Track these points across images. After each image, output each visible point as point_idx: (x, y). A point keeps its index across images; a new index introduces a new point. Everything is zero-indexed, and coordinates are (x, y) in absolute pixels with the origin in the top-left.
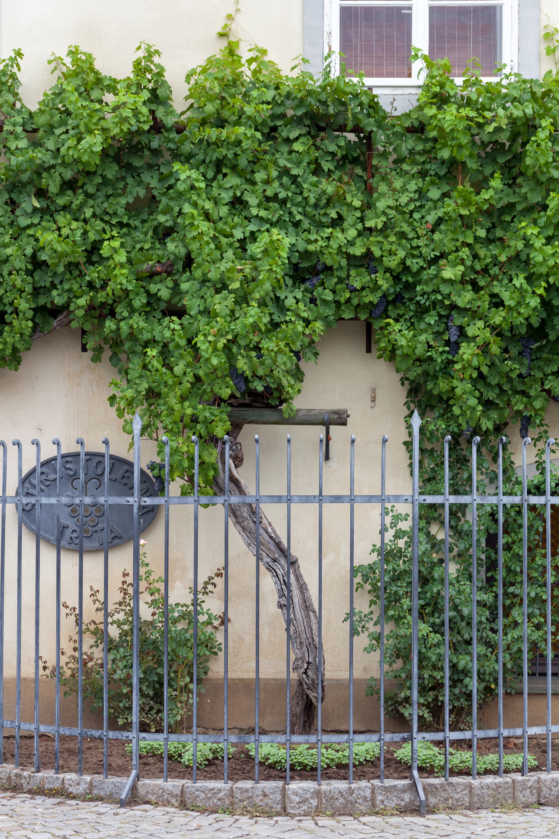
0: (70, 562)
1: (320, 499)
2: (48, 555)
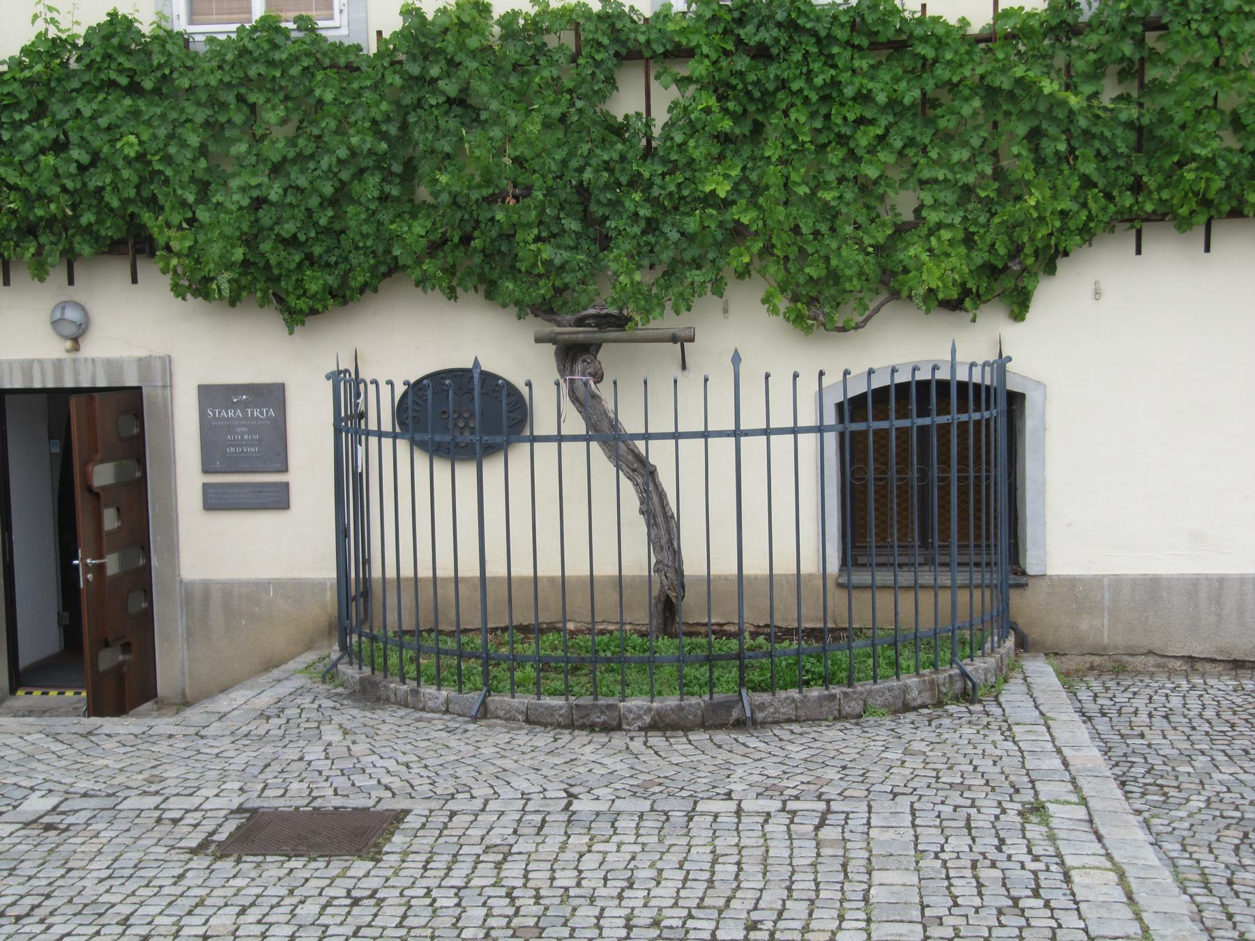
0: (442, 469)
1: (706, 435)
2: (422, 461)
